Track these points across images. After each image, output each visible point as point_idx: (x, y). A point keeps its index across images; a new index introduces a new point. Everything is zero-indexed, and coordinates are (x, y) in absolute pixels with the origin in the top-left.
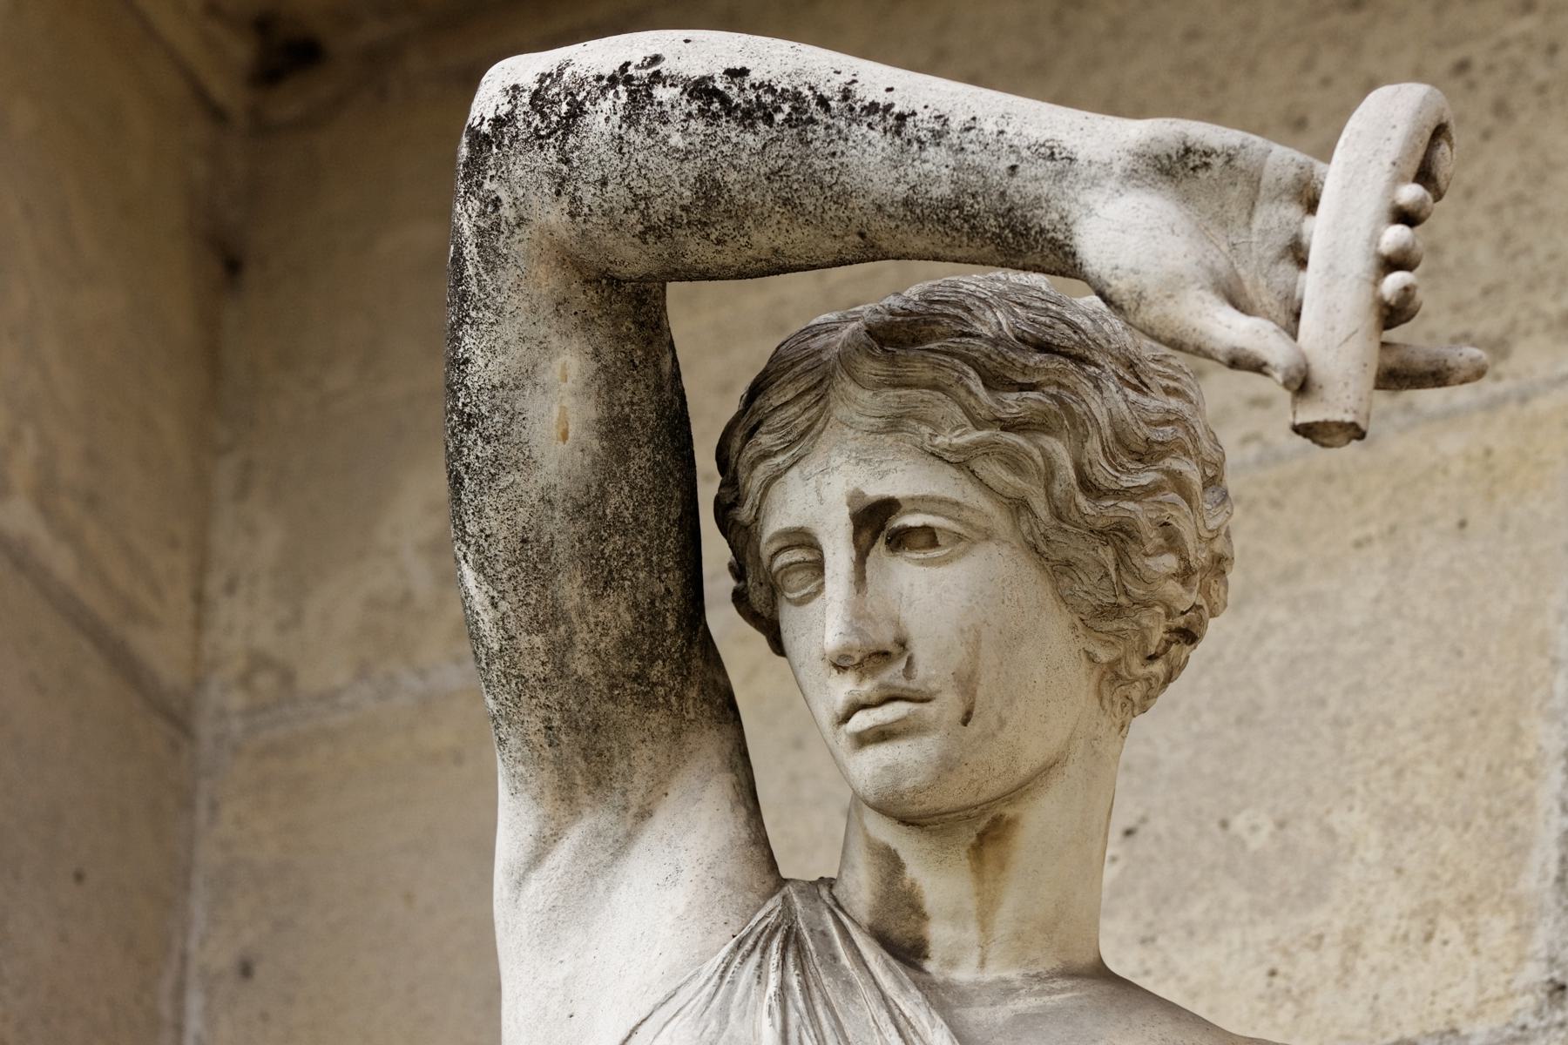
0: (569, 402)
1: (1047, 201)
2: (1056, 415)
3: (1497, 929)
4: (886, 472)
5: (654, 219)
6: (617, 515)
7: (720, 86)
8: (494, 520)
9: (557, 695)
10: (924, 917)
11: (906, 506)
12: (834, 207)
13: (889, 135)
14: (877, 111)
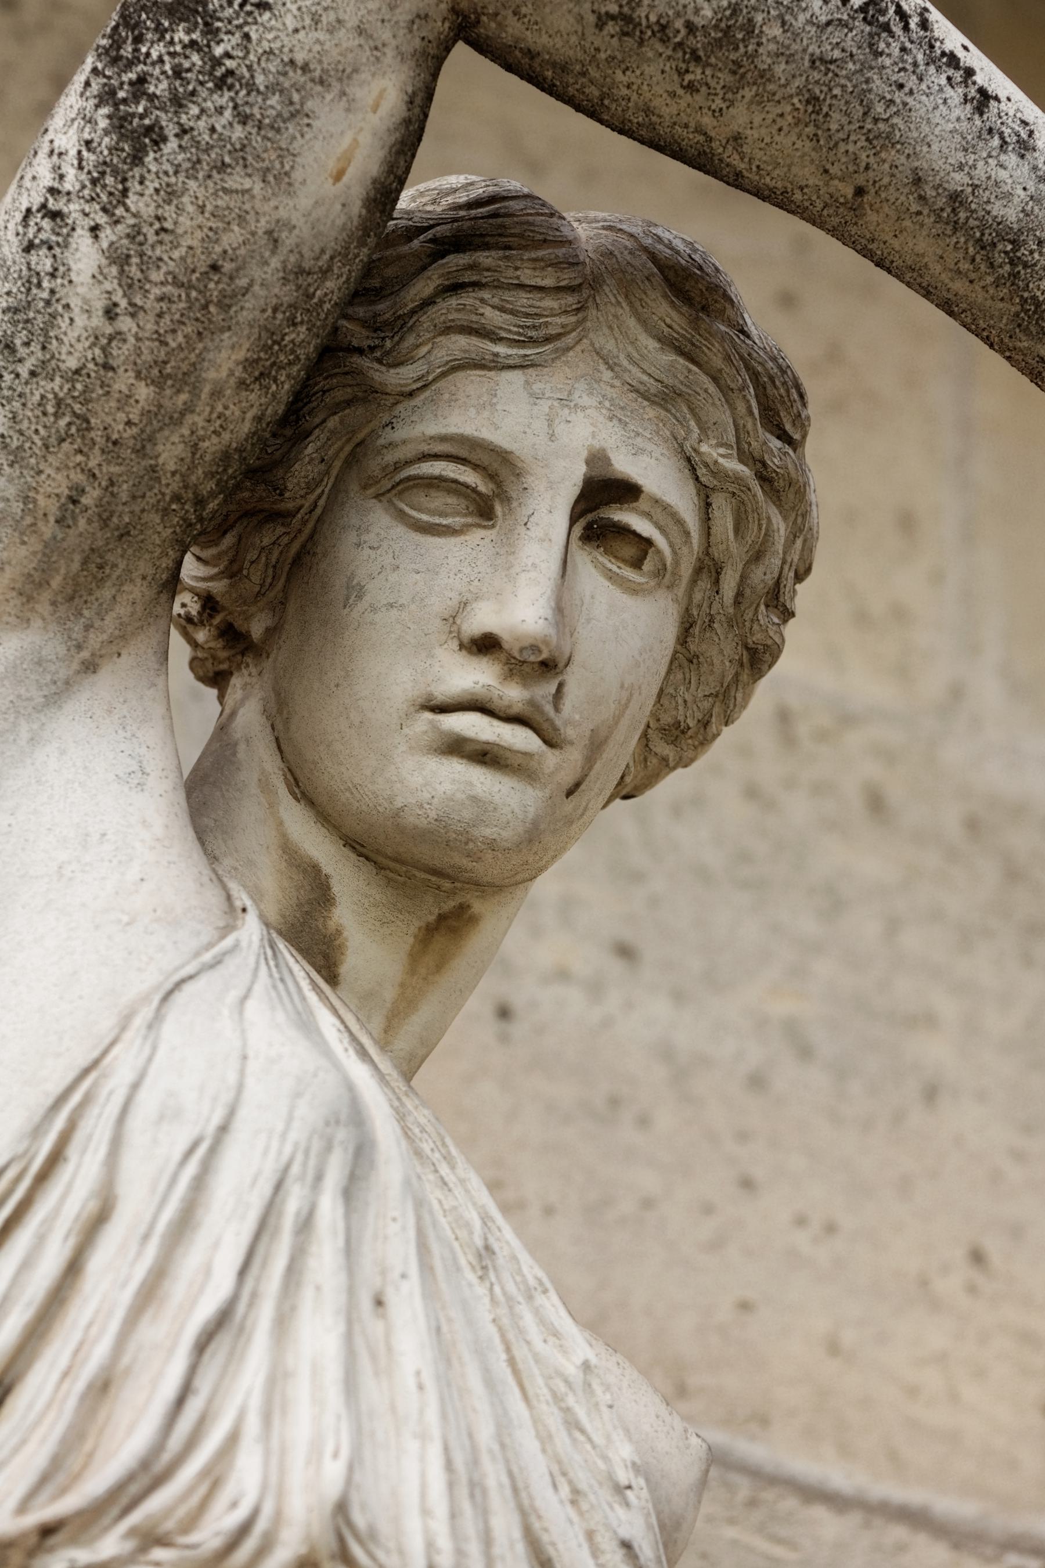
0: (366, 139)
9: (115, 469)
11: (643, 504)
12: (863, 143)
13: (968, 106)
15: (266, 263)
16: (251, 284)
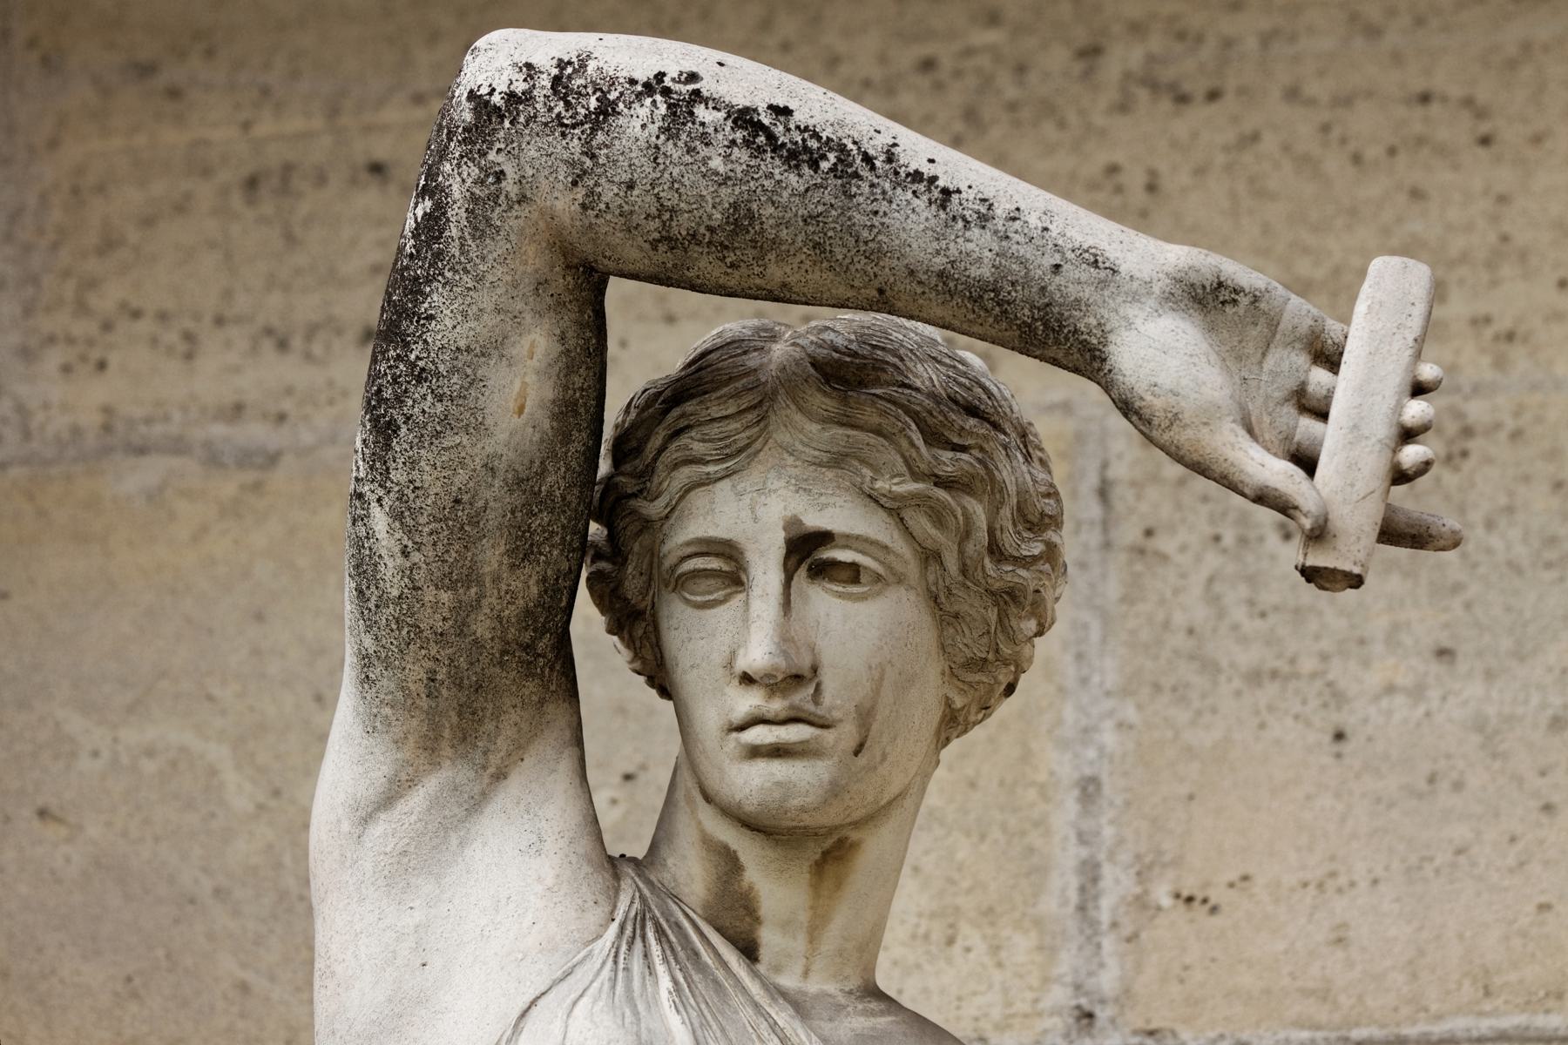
0: (531, 378)
1: (1087, 305)
2: (983, 480)
3: (1022, 946)
4: (826, 505)
5: (675, 231)
6: (550, 493)
7: (766, 121)
8: (426, 470)
10: (757, 920)
11: (839, 541)
12: (864, 261)
14: (921, 180)
15: (492, 486)
16: (487, 503)
